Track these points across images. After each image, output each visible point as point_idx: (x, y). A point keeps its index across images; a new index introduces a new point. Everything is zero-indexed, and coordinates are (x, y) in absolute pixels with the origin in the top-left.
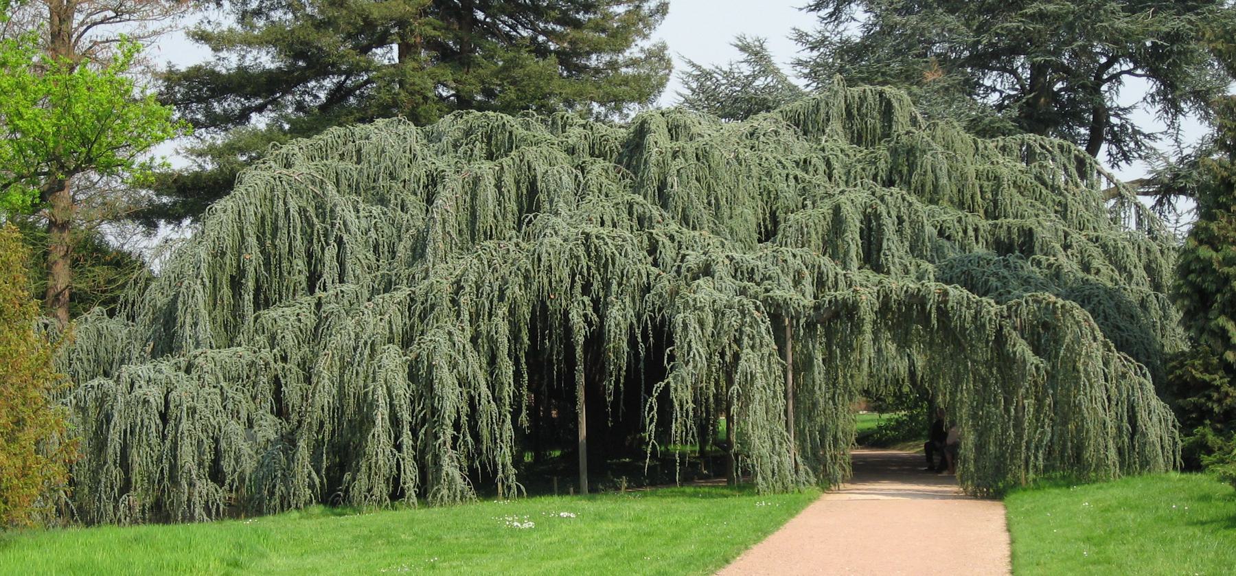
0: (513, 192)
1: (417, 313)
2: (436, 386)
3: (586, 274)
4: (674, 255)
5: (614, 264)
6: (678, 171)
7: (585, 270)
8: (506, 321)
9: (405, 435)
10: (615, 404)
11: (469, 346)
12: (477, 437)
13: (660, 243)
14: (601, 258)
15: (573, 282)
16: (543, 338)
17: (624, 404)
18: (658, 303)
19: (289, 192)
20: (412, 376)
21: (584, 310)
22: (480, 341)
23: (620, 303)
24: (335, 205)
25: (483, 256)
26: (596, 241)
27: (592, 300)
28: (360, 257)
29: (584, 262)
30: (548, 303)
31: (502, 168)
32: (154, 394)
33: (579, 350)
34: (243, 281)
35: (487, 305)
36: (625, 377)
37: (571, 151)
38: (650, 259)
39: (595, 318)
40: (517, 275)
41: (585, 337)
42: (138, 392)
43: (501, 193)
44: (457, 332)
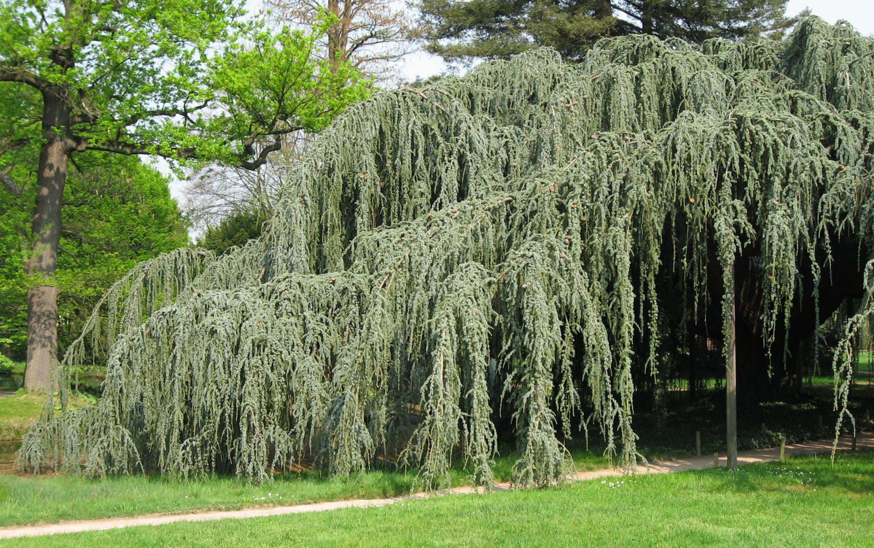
0: (656, 99)
1: (516, 223)
2: (526, 318)
3: (738, 172)
4: (858, 144)
5: (776, 157)
6: (850, 66)
7: (737, 164)
8: (628, 233)
9: (476, 385)
10: (777, 347)
11: (577, 265)
12: (585, 390)
13: (840, 129)
14: (758, 149)
15: (721, 179)
16: (680, 256)
17: (789, 347)
18: (840, 206)
19: (412, 109)
20: (498, 304)
21: (736, 217)
22: (593, 258)
23: (785, 207)
24: (460, 122)
25: (600, 148)
26: (753, 127)
27: (747, 204)
28: (485, 177)
29: (735, 153)
30: (686, 209)
31: (642, 73)
32: (224, 323)
33: (728, 273)
34: (357, 203)
35: (604, 210)
36: (792, 310)
37: (724, 66)
38: (826, 151)
39: (750, 229)
40: (643, 171)
41: (737, 254)
42: (207, 321)
43: (638, 97)
44: (559, 246)
